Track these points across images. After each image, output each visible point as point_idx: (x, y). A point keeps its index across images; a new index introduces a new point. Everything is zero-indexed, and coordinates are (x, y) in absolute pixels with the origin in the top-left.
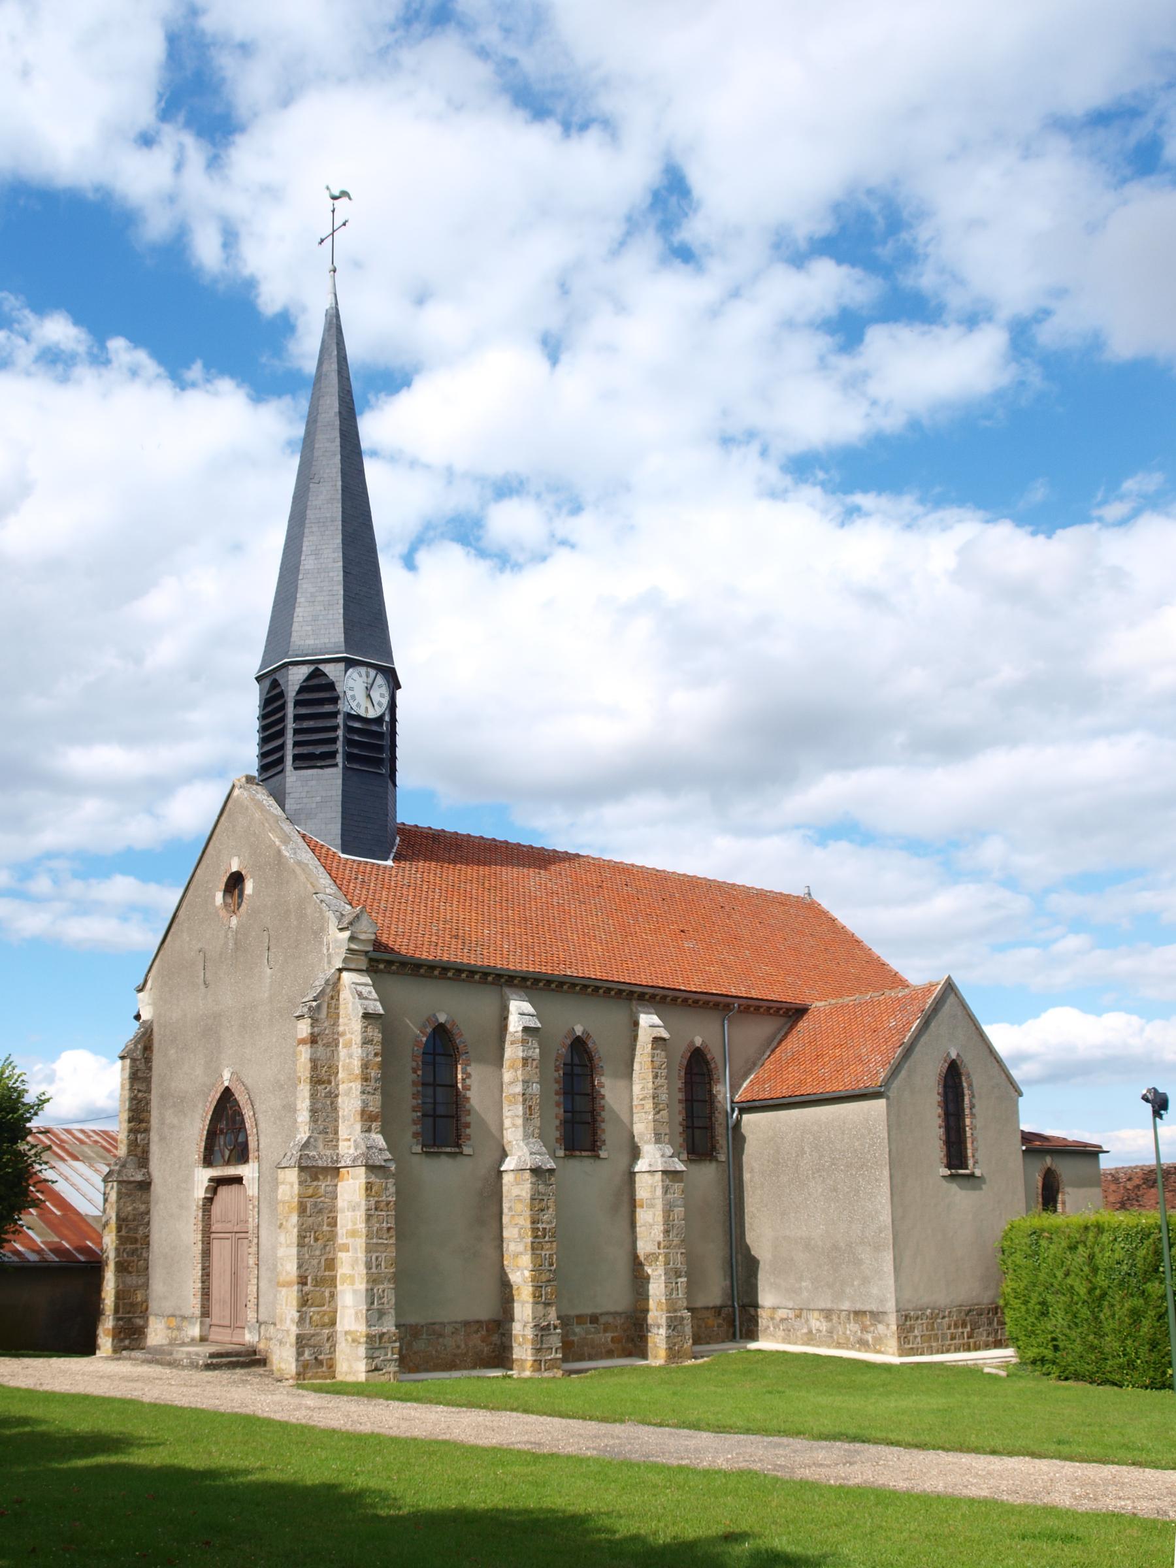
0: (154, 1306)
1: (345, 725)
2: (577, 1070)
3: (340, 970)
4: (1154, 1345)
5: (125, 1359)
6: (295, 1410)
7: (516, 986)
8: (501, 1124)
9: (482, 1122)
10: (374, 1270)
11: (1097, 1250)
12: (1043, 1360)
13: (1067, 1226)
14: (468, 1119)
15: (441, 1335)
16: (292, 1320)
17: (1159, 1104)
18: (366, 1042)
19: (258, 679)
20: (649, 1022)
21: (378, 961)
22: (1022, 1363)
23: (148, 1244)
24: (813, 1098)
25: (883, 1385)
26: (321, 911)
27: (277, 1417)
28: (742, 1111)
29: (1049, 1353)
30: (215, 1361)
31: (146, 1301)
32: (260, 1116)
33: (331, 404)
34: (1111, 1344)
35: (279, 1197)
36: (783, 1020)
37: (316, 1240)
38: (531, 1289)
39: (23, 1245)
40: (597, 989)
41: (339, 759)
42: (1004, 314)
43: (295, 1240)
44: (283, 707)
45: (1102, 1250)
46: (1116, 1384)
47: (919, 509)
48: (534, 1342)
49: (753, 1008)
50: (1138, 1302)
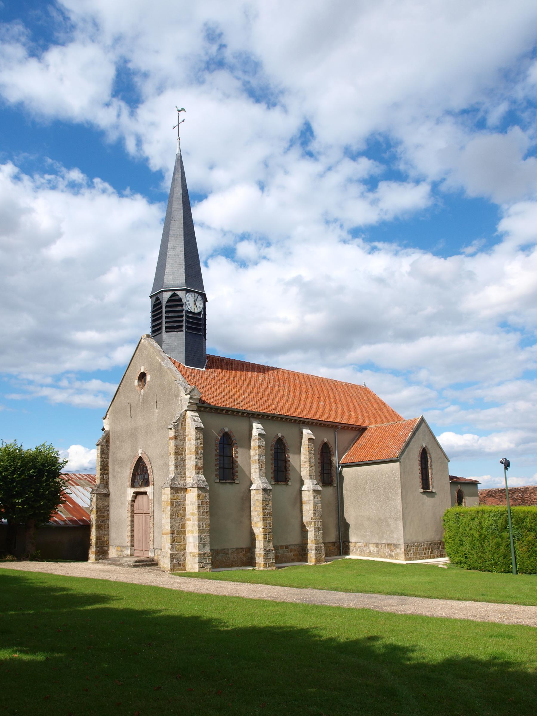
0: (111, 542)
1: (186, 315)
2: (279, 451)
3: (186, 411)
4: (505, 556)
5: (101, 563)
6: (173, 584)
7: (255, 418)
8: (250, 471)
9: (243, 471)
10: (201, 528)
11: (482, 520)
12: (461, 562)
13: (470, 511)
14: (237, 469)
15: (228, 554)
16: (169, 548)
17: (507, 465)
18: (197, 439)
19: (151, 297)
20: (307, 433)
21: (201, 407)
22: (452, 563)
23: (109, 518)
24: (371, 462)
25: (402, 572)
26: (178, 387)
27: (166, 587)
28: (343, 467)
29: (463, 560)
30: (137, 564)
31: (108, 540)
32: (154, 468)
33: (178, 206)
34: (488, 556)
35: (163, 500)
36: (358, 432)
37: (178, 516)
38: (263, 535)
39: (58, 518)
40: (286, 419)
41: (184, 328)
42: (429, 180)
43: (169, 516)
44: (161, 308)
45: (484, 520)
46: (489, 571)
47: (399, 248)
48: (264, 556)
49: (346, 428)
50: (499, 540)
